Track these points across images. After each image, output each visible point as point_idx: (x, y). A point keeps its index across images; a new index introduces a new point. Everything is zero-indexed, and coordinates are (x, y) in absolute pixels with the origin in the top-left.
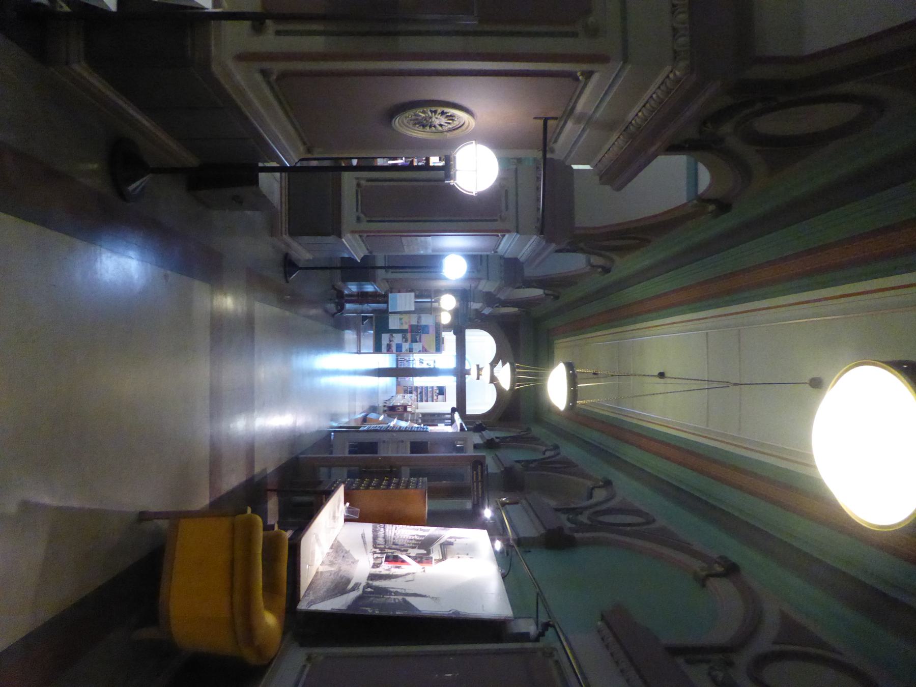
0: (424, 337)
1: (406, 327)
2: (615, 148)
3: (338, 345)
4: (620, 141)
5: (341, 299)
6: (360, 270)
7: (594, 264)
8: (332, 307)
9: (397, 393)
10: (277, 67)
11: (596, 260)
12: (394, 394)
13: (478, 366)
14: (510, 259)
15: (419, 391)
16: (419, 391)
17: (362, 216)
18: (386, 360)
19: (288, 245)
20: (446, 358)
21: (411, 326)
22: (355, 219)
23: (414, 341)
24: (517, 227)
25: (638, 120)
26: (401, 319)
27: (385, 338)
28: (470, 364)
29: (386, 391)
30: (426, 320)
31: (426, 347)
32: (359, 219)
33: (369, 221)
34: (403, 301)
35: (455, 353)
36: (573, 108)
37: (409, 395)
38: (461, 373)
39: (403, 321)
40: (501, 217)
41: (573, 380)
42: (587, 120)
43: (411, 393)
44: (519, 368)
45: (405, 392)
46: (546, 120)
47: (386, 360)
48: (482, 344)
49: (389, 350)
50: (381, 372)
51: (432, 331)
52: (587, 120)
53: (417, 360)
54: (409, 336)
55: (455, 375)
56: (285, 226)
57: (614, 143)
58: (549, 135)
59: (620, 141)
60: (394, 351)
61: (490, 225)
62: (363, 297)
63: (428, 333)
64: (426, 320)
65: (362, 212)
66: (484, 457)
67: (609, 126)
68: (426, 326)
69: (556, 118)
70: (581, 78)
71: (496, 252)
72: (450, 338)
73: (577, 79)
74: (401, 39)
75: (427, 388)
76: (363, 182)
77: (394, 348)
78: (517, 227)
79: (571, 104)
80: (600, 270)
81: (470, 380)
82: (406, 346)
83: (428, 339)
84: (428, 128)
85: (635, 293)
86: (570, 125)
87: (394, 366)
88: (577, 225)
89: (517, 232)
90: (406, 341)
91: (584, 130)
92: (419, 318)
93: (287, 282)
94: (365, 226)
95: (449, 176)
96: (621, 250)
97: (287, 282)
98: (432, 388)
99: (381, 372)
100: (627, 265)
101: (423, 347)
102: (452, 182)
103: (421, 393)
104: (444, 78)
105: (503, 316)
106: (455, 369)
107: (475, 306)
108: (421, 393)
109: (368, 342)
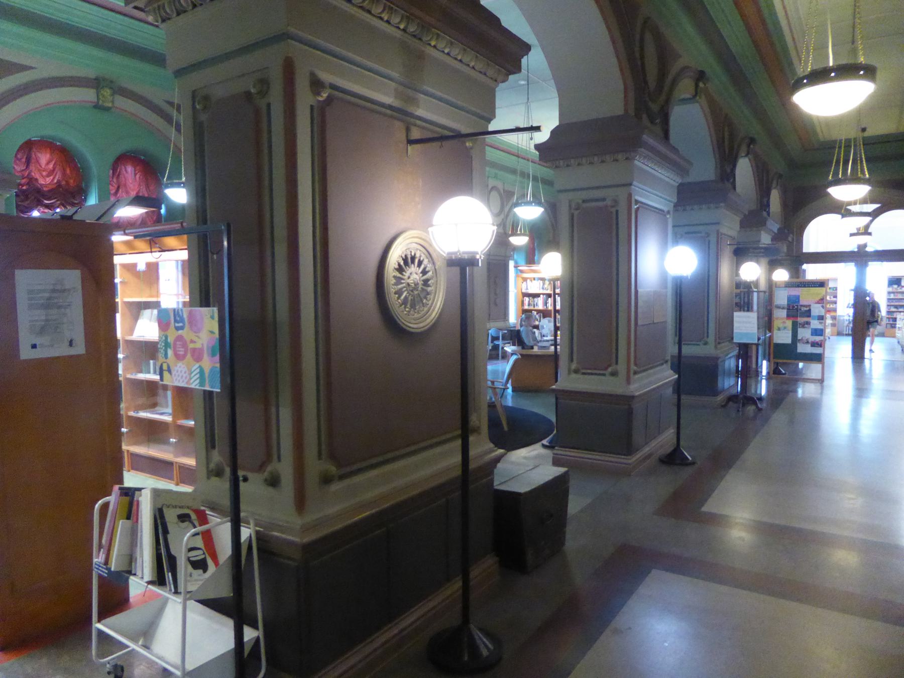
0: (803, 301)
1: (789, 323)
2: (455, 52)
3: (813, 406)
4: (441, 46)
5: (746, 399)
6: (696, 377)
7: (694, 93)
8: (751, 409)
9: (894, 337)
10: (315, 466)
11: (685, 88)
12: (895, 341)
13: (852, 235)
14: (678, 198)
15: (893, 309)
16: (893, 309)
17: (610, 370)
18: (840, 351)
19: (649, 456)
20: (842, 277)
21: (788, 317)
22: (612, 378)
23: (808, 313)
24: (624, 185)
25: (395, 20)
26: (779, 329)
27: (802, 348)
28: (851, 245)
29: (892, 351)
30: (781, 298)
31: (818, 299)
32: (614, 374)
33: (617, 363)
34: (746, 326)
35: (842, 265)
36: (390, 107)
37: (898, 322)
38: (860, 257)
39: (781, 326)
40: (612, 207)
41: (820, 76)
42: (410, 88)
43: (895, 320)
44: (836, 173)
45: (893, 326)
46: (411, 142)
47: (840, 351)
48: (822, 233)
49: (820, 345)
50: (858, 355)
51: (795, 292)
52: (410, 88)
53: (845, 310)
54: (801, 320)
55: (866, 265)
56: (622, 459)
57: (442, 51)
58: (429, 135)
59: (441, 46)
60: (821, 338)
61: (623, 217)
62: (748, 373)
63: (798, 297)
64: (781, 298)
65: (606, 369)
66: (527, 48)
67: (415, 61)
68: (789, 299)
69: (408, 130)
70: (325, 95)
71: (668, 212)
72: (813, 271)
73: (330, 100)
74: (278, 320)
75: (889, 300)
76: (574, 366)
77: (818, 339)
78: (624, 185)
79: (389, 112)
80: (701, 85)
81: (873, 244)
82: (815, 324)
83: (807, 297)
84: (429, 289)
85: (734, 35)
86: (420, 112)
87: (850, 338)
88: (620, 111)
89: (631, 184)
90: (808, 323)
91: (426, 94)
92: (778, 307)
93: (693, 463)
94: (621, 367)
95: (472, 262)
96: (665, 55)
97: (693, 463)
98: (889, 293)
99: (858, 355)
100: (691, 49)
101: (818, 303)
102: (480, 257)
103: (896, 307)
104: (332, 269)
105: (785, 205)
106: (856, 265)
107: (765, 239)
108: (896, 307)
109: (813, 370)
